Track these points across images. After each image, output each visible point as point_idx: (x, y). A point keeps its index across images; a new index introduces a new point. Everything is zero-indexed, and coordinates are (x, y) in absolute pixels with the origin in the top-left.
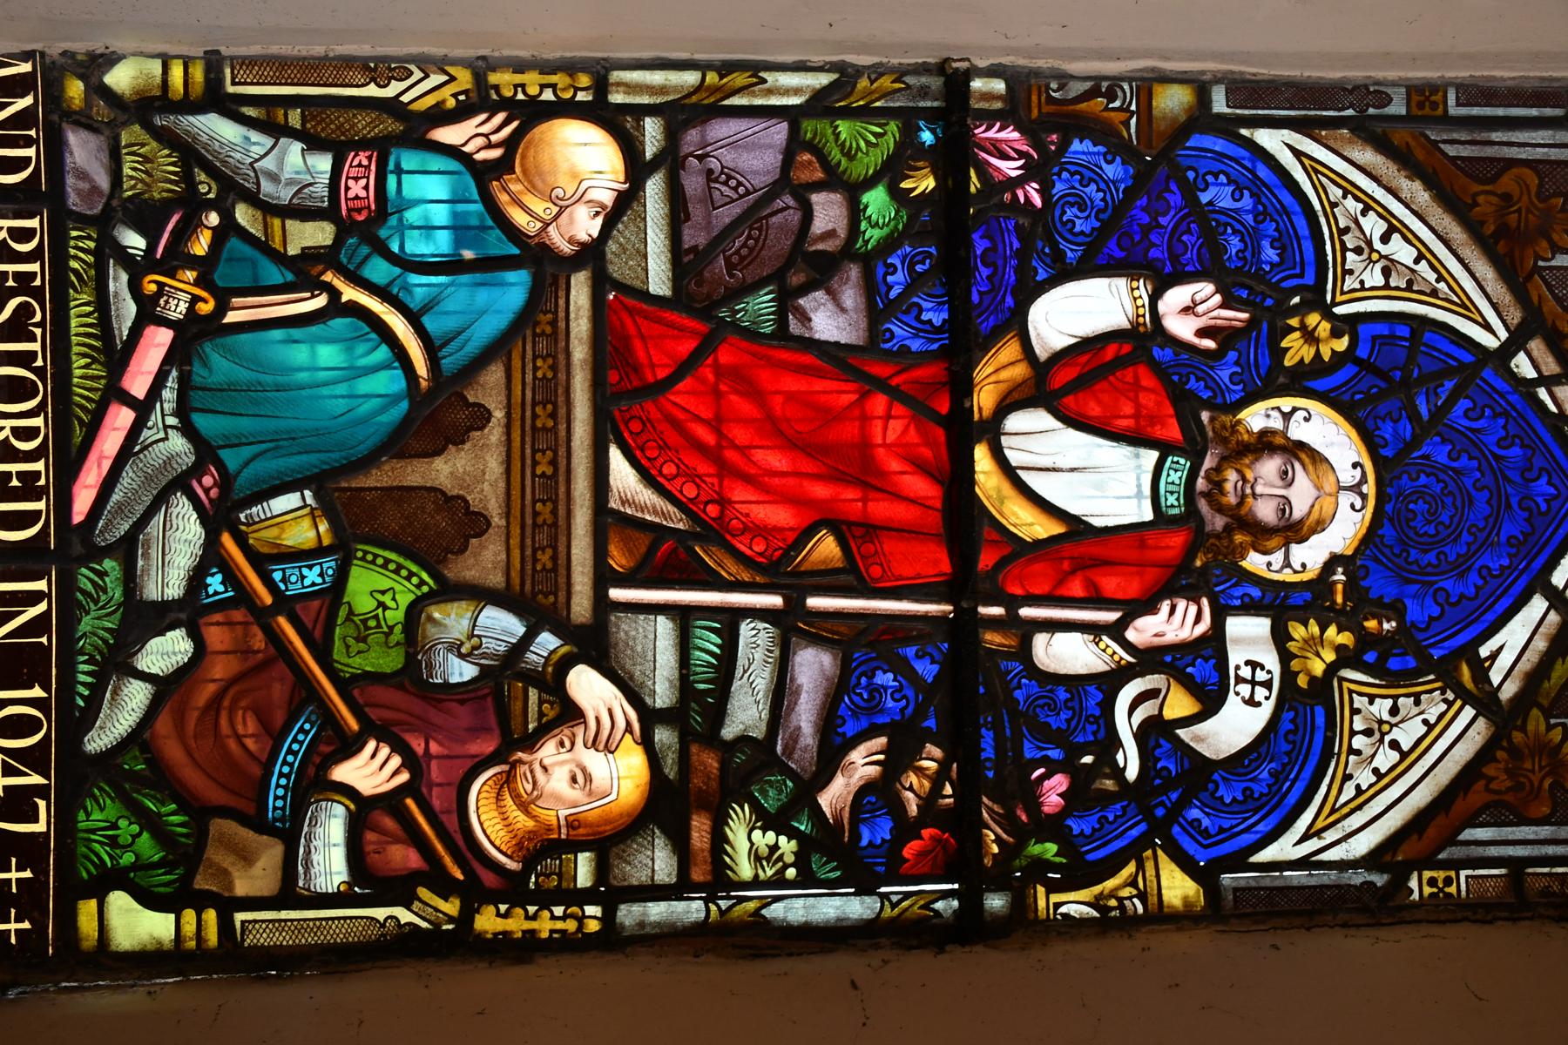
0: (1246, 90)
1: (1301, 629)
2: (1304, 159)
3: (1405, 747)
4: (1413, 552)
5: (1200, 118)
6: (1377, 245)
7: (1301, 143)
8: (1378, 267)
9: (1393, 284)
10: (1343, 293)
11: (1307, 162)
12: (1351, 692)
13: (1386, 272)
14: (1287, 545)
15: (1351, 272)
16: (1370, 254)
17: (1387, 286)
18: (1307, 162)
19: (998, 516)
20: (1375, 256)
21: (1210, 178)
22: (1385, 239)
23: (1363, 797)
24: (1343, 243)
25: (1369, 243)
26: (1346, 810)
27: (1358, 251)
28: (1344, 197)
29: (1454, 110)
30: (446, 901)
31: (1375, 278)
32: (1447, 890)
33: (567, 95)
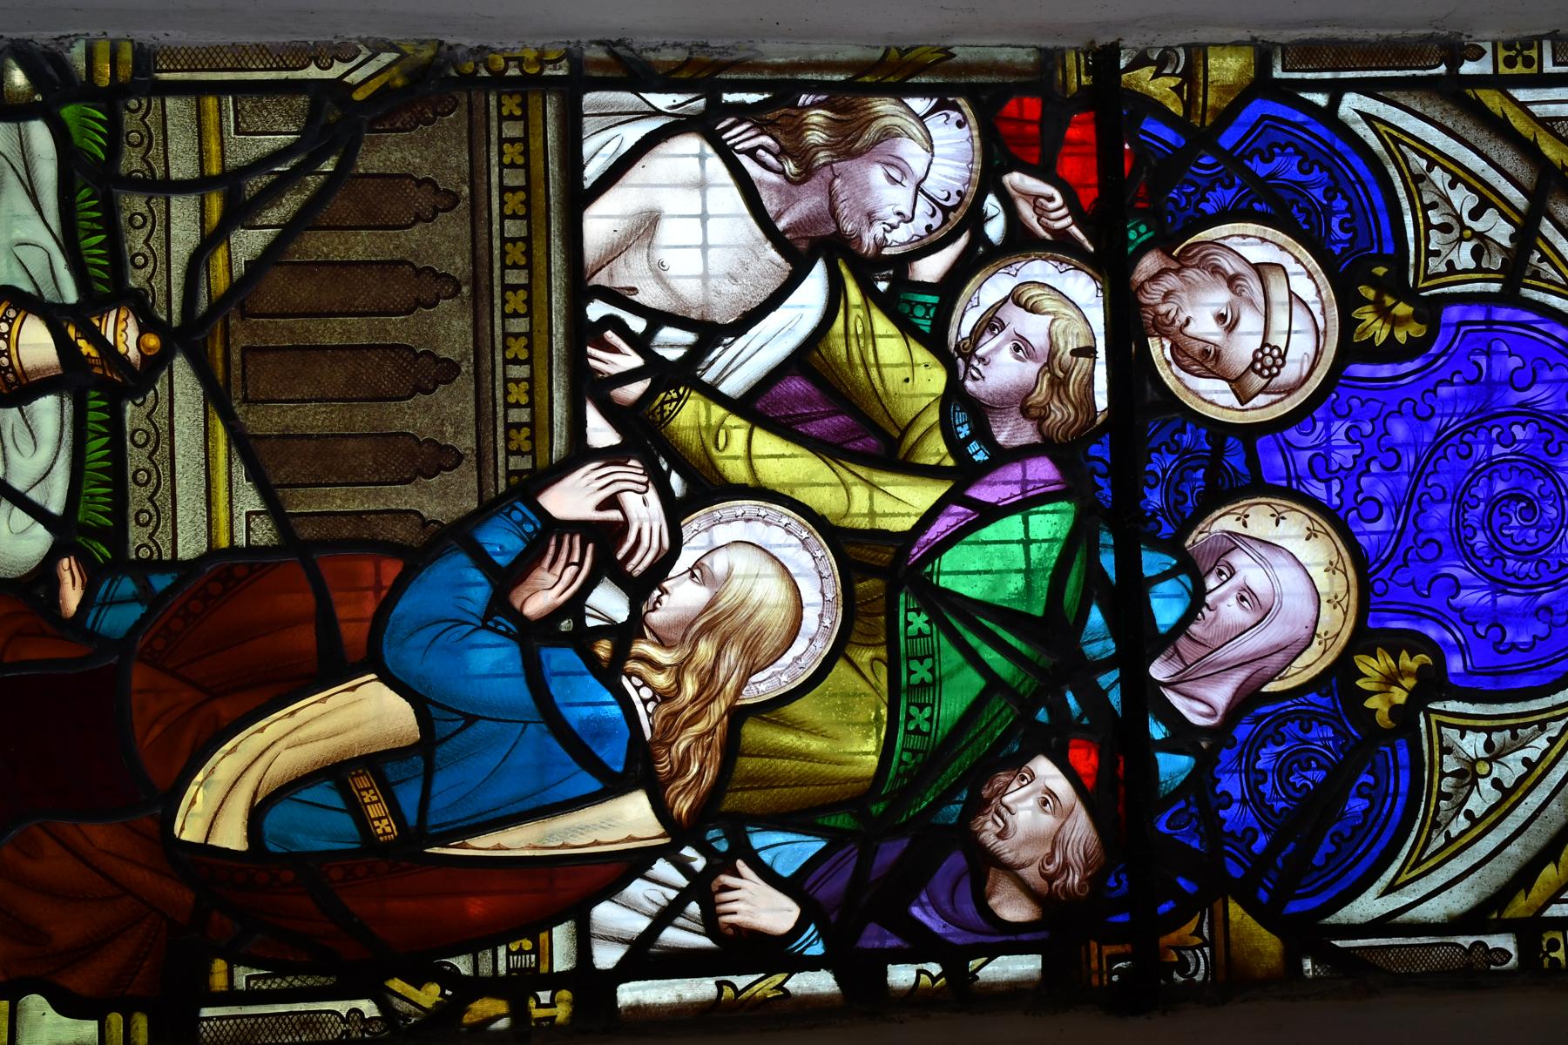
0: (1306, 53)
1: (1372, 662)
2: (1378, 125)
3: (1508, 784)
4: (1510, 563)
5: (1260, 85)
6: (1467, 221)
7: (1401, 119)
8: (1467, 247)
9: (509, 246)
10: (1427, 278)
11: (1382, 128)
12: (1440, 724)
13: (1477, 254)
14: (725, 837)
15: (1437, 253)
16: (1461, 233)
17: (1478, 269)
18: (1382, 128)
19: (228, 746)
20: (1468, 233)
21: (1276, 150)
22: (1476, 214)
23: (1452, 847)
24: (1426, 218)
25: (1459, 218)
26: (1431, 863)
27: (1445, 228)
28: (1430, 168)
29: (1549, 67)
30: (419, 989)
31: (1464, 257)
32: (1553, 955)
33: (534, 70)
